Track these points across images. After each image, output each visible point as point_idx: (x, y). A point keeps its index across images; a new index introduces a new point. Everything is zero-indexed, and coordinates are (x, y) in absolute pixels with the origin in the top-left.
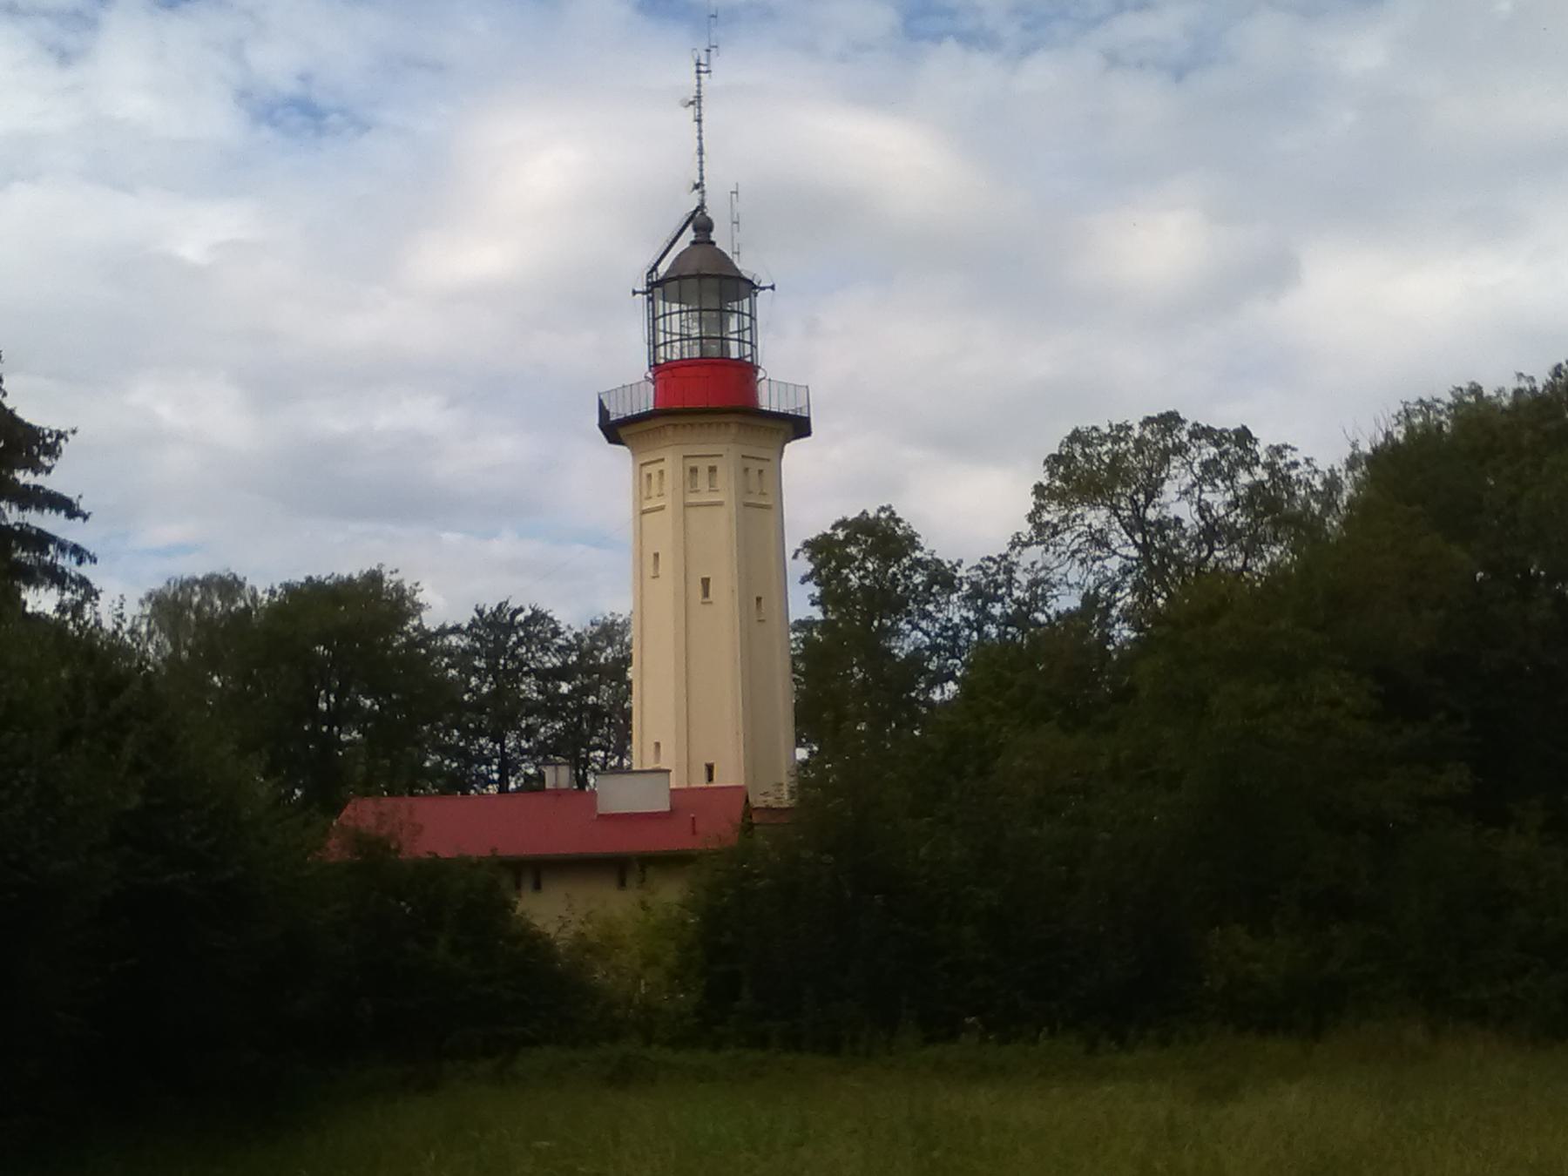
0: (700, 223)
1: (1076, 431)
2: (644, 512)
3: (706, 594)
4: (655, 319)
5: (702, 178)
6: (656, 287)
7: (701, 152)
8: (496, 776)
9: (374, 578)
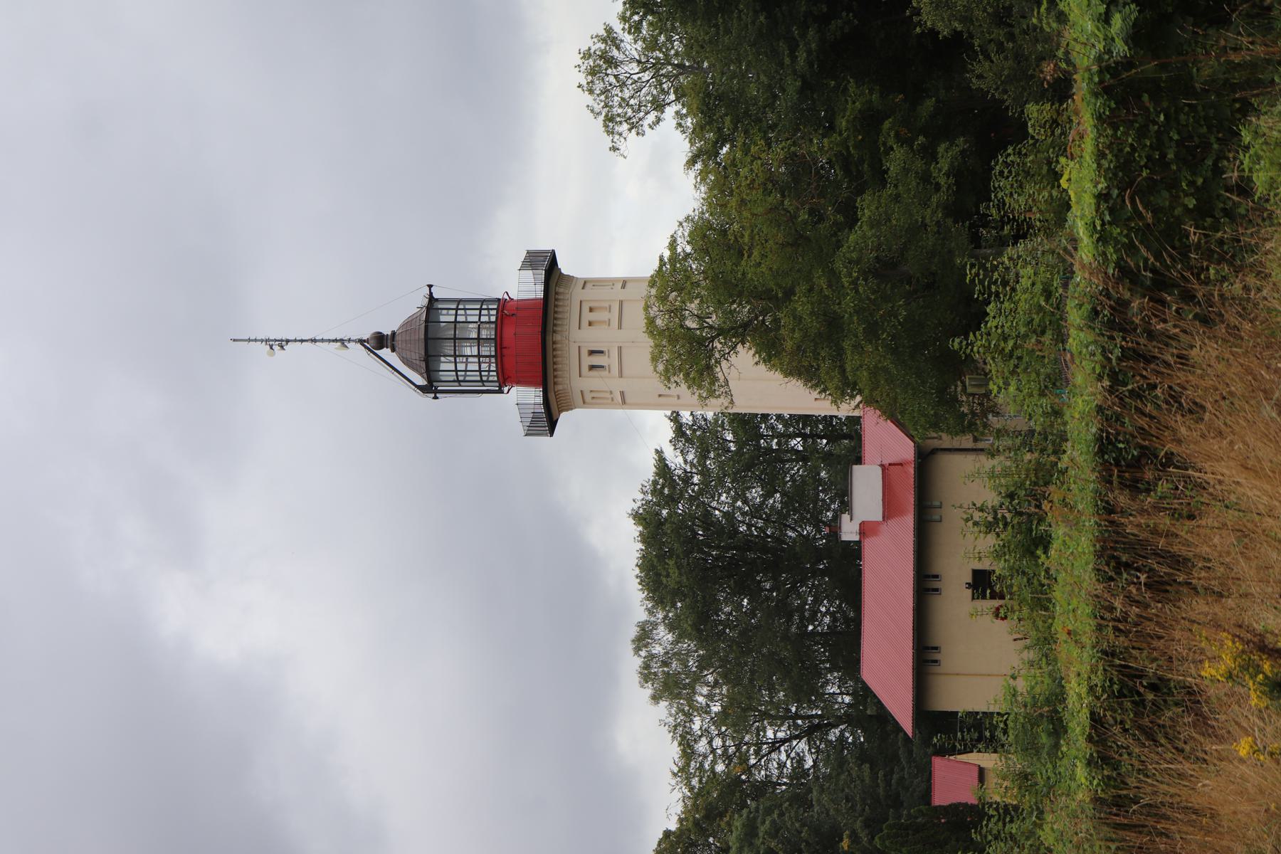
0: (380, 341)
2: (624, 402)
5: (336, 341)
6: (431, 388)
7: (314, 341)
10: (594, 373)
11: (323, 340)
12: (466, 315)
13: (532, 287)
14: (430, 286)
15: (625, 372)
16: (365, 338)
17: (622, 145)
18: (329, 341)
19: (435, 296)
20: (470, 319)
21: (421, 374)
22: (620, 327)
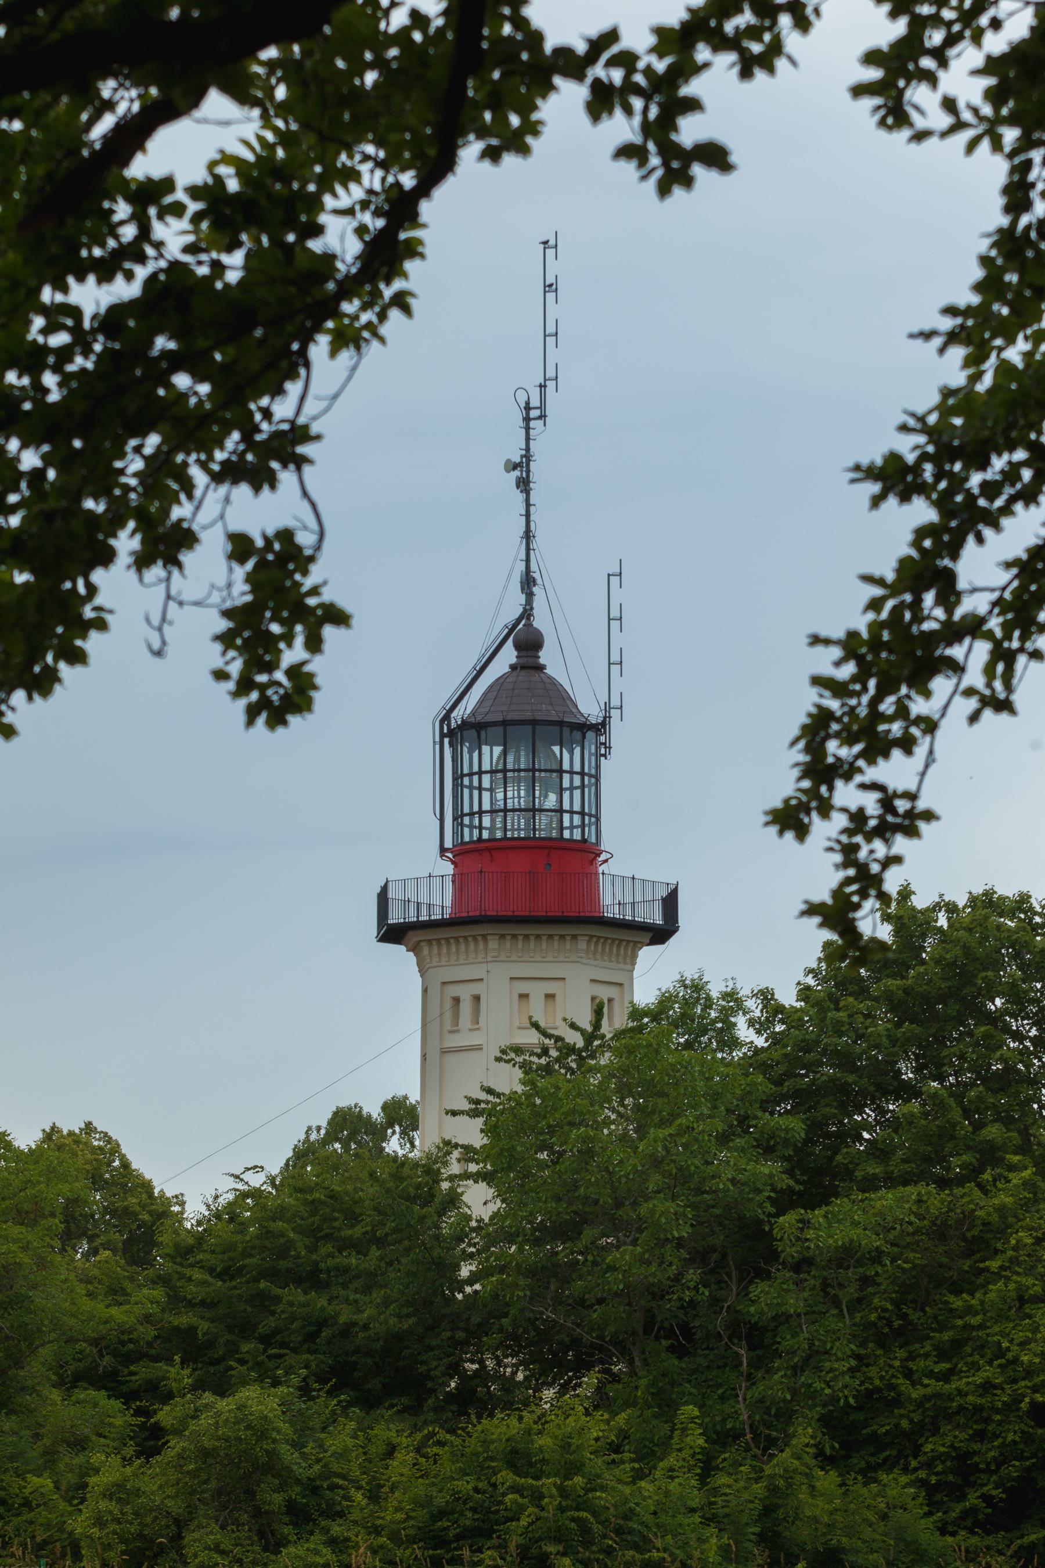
0: (529, 644)
1: (524, 150)
6: (458, 733)
10: (448, 1004)
12: (572, 788)
20: (566, 795)
21: (473, 713)
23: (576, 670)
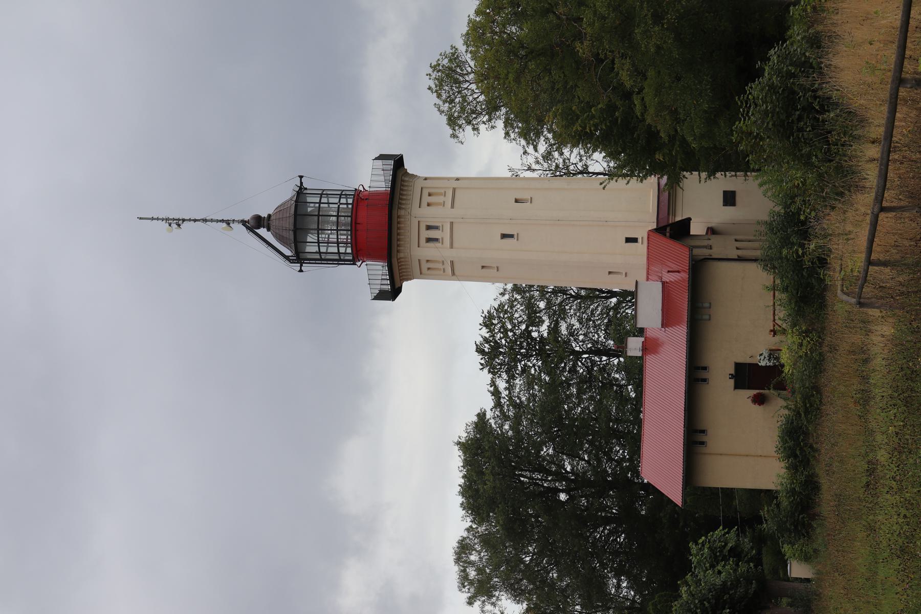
0: (256, 224)
2: (453, 273)
3: (511, 236)
4: (321, 259)
5: (222, 221)
6: (299, 258)
7: (205, 220)
8: (604, 358)
9: (465, 447)
10: (431, 244)
11: (212, 221)
13: (383, 184)
14: (301, 177)
15: (455, 245)
16: (246, 219)
17: (461, 135)
18: (218, 221)
19: (305, 185)
20: (331, 200)
22: (452, 207)
23: (270, 199)
